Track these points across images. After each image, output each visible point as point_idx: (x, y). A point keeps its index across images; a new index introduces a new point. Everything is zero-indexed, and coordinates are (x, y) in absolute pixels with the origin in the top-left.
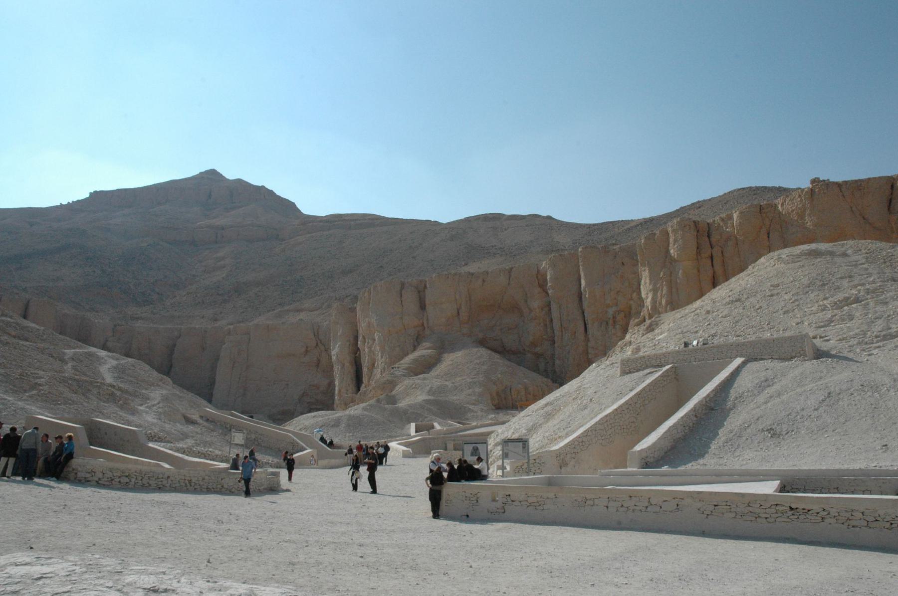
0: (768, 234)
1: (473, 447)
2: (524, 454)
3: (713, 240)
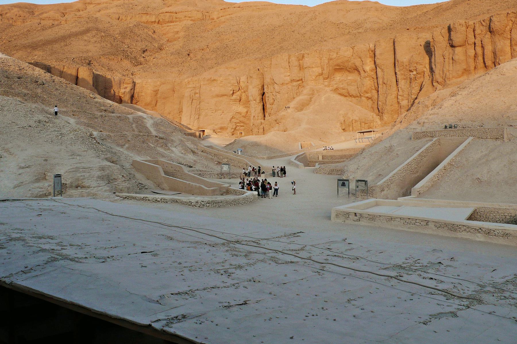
0: (511, 31)
1: (342, 182)
2: (366, 187)
3: (476, 32)
